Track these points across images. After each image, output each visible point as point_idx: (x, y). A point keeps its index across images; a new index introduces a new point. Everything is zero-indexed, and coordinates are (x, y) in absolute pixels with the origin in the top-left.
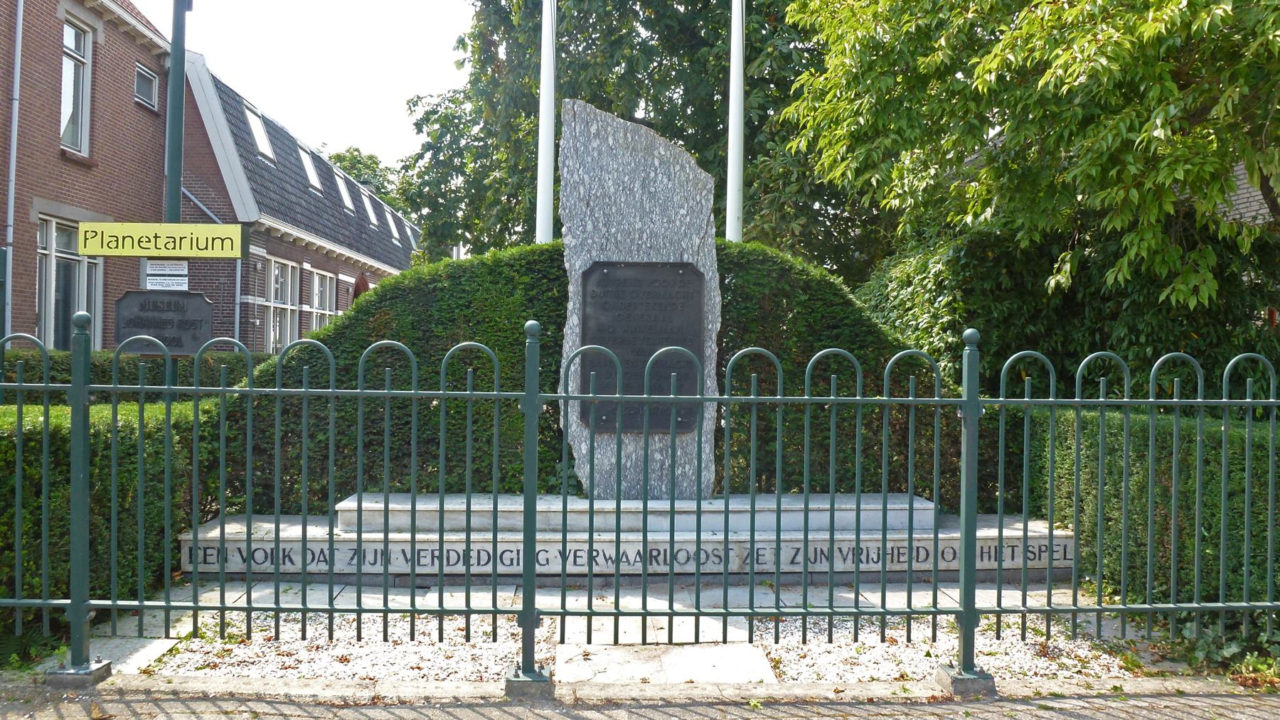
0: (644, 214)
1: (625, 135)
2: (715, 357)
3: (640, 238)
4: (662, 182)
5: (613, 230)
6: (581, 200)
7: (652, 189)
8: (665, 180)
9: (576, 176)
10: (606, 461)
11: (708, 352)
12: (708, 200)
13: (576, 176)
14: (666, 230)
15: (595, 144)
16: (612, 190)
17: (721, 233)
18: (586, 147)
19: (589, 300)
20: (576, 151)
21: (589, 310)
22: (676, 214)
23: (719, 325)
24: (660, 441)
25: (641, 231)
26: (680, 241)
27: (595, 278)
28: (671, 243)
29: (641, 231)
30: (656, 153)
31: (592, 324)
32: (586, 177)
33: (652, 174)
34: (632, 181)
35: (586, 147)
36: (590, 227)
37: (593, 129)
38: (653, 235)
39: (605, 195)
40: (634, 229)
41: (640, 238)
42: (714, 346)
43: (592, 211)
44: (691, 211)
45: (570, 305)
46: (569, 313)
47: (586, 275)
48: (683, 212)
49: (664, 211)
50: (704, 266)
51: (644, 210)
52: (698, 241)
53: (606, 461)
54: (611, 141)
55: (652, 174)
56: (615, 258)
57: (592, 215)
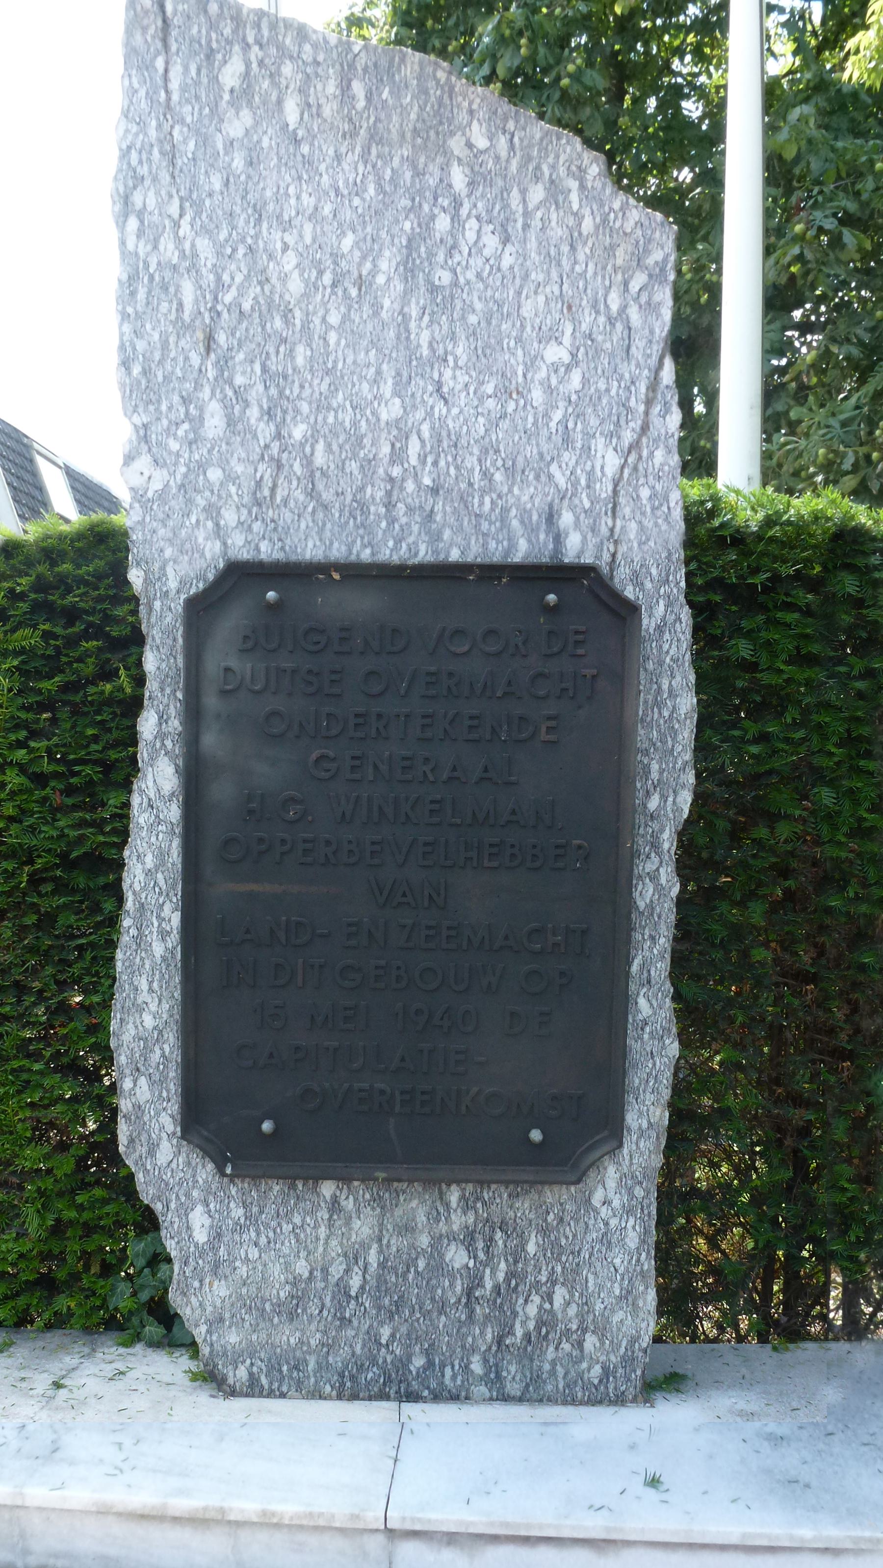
0: (415, 368)
1: (345, 87)
2: (668, 914)
3: (397, 456)
4: (477, 247)
5: (299, 432)
6: (183, 328)
7: (444, 277)
8: (491, 242)
9: (167, 246)
10: (276, 1271)
11: (644, 895)
12: (650, 308)
13: (167, 246)
14: (494, 424)
15: (237, 125)
16: (295, 286)
17: (699, 459)
18: (205, 141)
19: (211, 701)
20: (171, 156)
21: (211, 740)
22: (531, 364)
23: (686, 799)
24: (466, 1205)
25: (401, 432)
26: (545, 460)
27: (232, 622)
28: (510, 471)
29: (401, 432)
30: (456, 144)
31: (222, 792)
32: (204, 246)
33: (443, 223)
34: (370, 249)
35: (205, 141)
36: (214, 423)
37: (231, 74)
38: (445, 442)
39: (271, 306)
40: (375, 424)
41: (397, 456)
42: (668, 876)
43: (224, 364)
44: (587, 347)
45: (147, 725)
46: (143, 754)
47: (202, 609)
48: (556, 353)
49: (484, 353)
50: (636, 579)
51: (412, 353)
52: (612, 462)
53: (276, 1271)
54: (292, 112)
55: (443, 223)
56: (311, 550)
57: (224, 376)
